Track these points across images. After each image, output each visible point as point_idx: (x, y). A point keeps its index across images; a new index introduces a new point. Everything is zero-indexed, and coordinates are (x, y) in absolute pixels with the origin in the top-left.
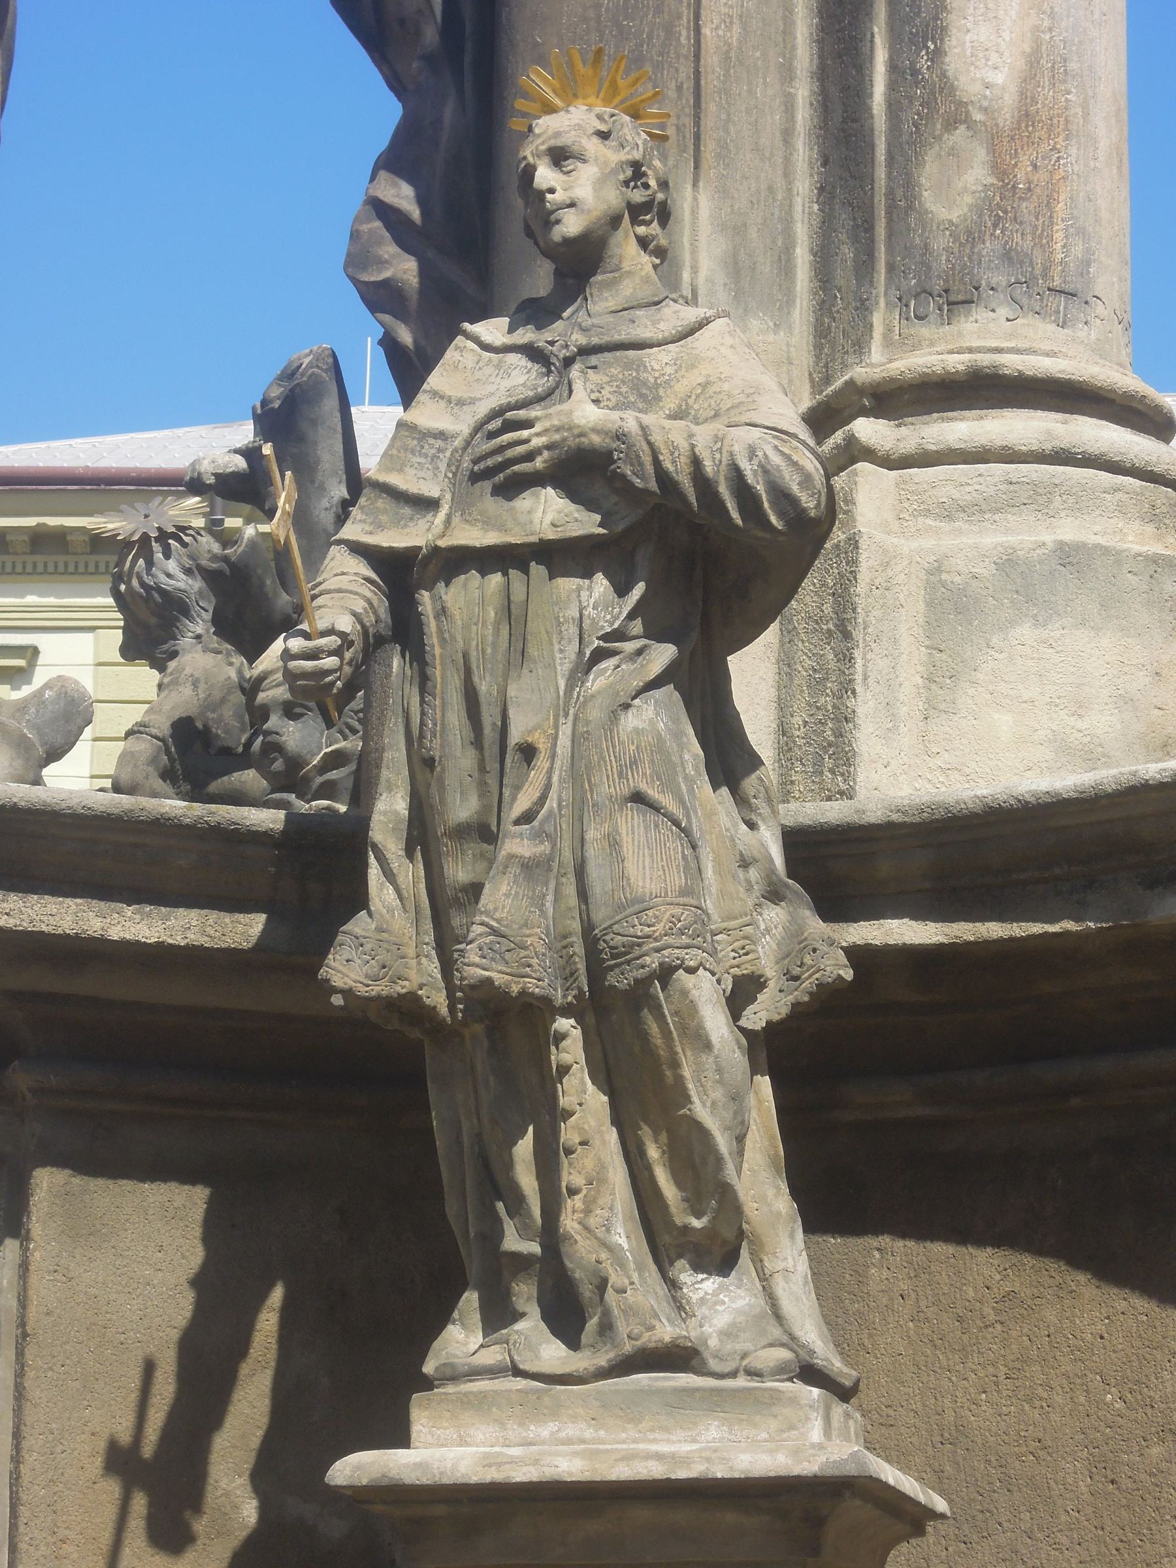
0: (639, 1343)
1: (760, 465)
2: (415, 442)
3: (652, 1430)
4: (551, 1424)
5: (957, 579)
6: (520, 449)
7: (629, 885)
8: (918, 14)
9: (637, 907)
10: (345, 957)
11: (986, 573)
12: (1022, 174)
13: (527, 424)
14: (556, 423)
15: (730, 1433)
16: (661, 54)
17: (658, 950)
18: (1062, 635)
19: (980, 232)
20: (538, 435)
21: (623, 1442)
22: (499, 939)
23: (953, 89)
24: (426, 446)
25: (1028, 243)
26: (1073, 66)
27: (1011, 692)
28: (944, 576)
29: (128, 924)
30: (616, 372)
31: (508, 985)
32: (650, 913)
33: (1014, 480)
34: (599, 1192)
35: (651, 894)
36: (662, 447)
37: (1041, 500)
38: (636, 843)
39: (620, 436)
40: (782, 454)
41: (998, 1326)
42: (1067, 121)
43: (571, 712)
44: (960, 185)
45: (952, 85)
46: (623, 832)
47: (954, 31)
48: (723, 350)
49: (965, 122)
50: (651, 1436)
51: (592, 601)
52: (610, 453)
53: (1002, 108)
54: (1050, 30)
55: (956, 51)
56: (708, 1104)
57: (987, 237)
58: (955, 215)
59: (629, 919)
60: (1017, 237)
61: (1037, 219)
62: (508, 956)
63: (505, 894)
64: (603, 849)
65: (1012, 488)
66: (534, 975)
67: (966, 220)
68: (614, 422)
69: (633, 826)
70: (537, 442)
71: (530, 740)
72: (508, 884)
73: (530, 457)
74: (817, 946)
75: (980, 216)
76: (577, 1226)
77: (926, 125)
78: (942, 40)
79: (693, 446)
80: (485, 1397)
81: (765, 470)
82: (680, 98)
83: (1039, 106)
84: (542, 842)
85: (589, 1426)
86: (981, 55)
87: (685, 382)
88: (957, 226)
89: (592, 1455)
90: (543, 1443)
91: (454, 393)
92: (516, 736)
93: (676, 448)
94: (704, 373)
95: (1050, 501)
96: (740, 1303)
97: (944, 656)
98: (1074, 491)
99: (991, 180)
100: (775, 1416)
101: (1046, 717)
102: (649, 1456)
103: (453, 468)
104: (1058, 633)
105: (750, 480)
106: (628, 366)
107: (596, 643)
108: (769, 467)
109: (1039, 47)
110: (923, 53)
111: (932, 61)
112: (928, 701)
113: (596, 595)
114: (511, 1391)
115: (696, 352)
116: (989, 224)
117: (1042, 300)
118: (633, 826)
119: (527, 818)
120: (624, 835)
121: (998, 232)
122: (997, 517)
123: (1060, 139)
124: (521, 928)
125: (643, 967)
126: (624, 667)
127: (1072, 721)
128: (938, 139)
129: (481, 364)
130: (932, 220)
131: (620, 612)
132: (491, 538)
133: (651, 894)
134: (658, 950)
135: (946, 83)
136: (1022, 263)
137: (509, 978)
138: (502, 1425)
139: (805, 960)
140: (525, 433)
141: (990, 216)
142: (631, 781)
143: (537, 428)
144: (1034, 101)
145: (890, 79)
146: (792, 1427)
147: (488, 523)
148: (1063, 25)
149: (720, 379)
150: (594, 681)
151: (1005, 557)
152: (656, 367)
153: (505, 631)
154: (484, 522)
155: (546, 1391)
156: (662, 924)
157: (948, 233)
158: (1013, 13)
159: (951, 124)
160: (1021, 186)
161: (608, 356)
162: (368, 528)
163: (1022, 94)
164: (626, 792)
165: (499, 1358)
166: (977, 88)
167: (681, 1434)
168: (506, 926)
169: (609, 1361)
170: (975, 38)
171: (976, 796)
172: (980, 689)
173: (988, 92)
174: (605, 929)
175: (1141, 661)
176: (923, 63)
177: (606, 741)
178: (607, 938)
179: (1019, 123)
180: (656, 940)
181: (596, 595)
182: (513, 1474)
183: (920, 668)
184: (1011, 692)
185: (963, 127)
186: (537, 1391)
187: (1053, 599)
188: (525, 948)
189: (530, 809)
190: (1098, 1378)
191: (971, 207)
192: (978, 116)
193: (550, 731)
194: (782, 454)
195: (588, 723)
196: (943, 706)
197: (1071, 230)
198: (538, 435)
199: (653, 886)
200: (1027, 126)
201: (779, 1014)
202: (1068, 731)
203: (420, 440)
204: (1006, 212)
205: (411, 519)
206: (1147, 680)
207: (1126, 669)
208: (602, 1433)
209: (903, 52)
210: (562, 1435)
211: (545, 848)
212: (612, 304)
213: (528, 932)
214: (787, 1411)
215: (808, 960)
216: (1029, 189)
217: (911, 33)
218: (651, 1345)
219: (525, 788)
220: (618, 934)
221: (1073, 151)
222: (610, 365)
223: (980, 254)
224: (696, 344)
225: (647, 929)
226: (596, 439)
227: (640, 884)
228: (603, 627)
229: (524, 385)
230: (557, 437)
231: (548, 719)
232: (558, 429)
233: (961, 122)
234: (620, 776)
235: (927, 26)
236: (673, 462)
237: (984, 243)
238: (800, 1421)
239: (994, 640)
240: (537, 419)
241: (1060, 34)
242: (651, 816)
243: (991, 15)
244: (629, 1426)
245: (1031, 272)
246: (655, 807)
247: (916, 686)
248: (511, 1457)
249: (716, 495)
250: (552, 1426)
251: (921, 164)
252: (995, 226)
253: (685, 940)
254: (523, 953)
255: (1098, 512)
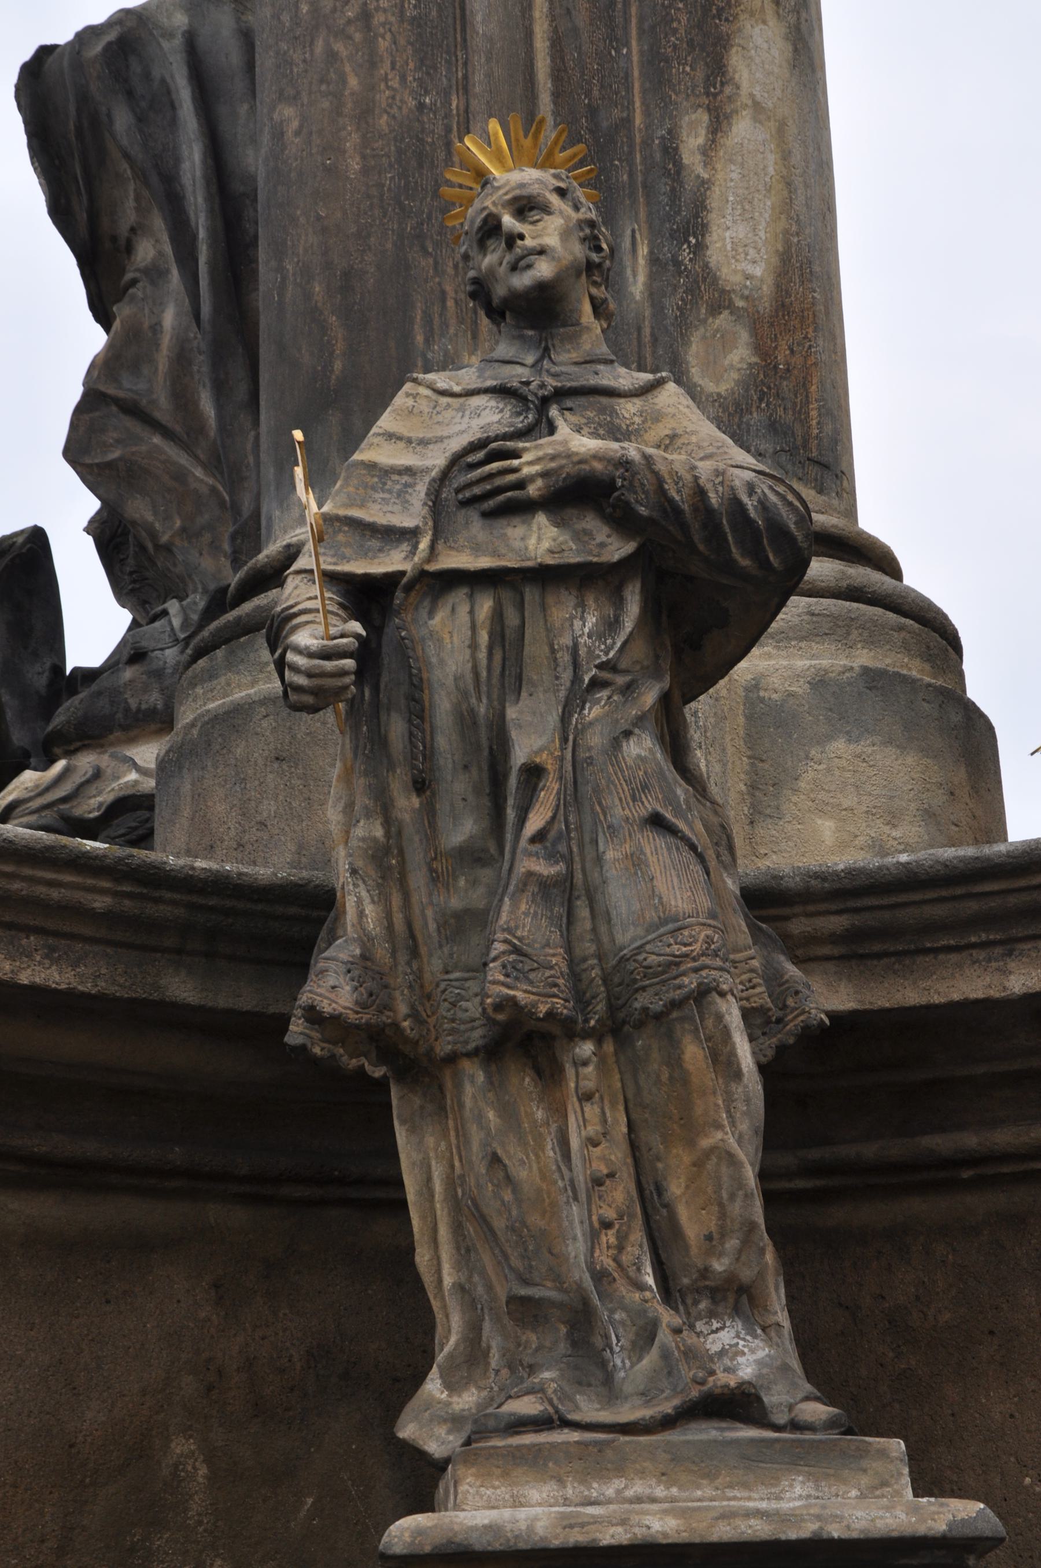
0: (705, 1388)
1: (760, 501)
2: (376, 479)
3: (731, 1486)
4: (617, 1481)
5: (774, 696)
6: (511, 478)
7: (662, 904)
8: (678, 213)
9: (671, 926)
10: (331, 983)
11: (800, 691)
12: (782, 356)
13: (516, 454)
14: (550, 451)
15: (817, 1490)
16: (440, 234)
17: (696, 970)
18: (874, 751)
19: (747, 404)
20: (530, 463)
21: (699, 1500)
22: (521, 958)
23: (715, 279)
24: (389, 483)
25: (790, 417)
26: (816, 268)
27: (831, 800)
28: (762, 694)
29: (37, 968)
30: (592, 415)
31: (534, 1005)
32: (686, 933)
33: (816, 612)
34: (629, 1227)
35: (684, 914)
36: (666, 476)
37: (840, 631)
38: (661, 863)
39: (625, 463)
40: (777, 493)
41: (897, 1406)
42: (814, 316)
43: (571, 737)
44: (727, 362)
45: (715, 275)
46: (648, 852)
47: (714, 228)
48: (681, 408)
49: (728, 307)
50: (730, 1493)
51: (586, 630)
52: (613, 481)
53: (761, 298)
54: (798, 234)
55: (717, 245)
56: (736, 1136)
57: (754, 409)
58: (723, 388)
59: (664, 938)
60: (780, 411)
61: (796, 397)
62: (532, 976)
63: (524, 913)
64: (627, 869)
65: (814, 619)
66: (561, 995)
67: (734, 393)
68: (616, 451)
69: (656, 847)
70: (526, 471)
71: (538, 760)
72: (527, 903)
73: (521, 485)
74: (800, 988)
75: (747, 390)
76: (611, 1263)
77: (691, 309)
78: (703, 236)
79: (696, 478)
80: (540, 1450)
81: (763, 505)
82: (456, 275)
83: (793, 299)
84: (557, 862)
85: (659, 1482)
86: (741, 250)
87: (653, 433)
88: (725, 398)
89: (682, 1513)
90: (609, 1502)
91: (417, 434)
92: (520, 755)
93: (680, 478)
94: (669, 426)
95: (848, 633)
96: (761, 1354)
97: (766, 766)
98: (868, 625)
99: (755, 359)
100: (865, 1471)
101: (864, 824)
102: (748, 1514)
103: (433, 497)
104: (870, 750)
105: (752, 514)
106: (602, 410)
107: (594, 671)
108: (768, 504)
109: (790, 247)
110: (685, 246)
111: (694, 253)
112: (753, 806)
113: (589, 625)
114: (568, 1443)
115: (658, 407)
116: (755, 397)
117: (803, 468)
118: (656, 847)
119: (539, 837)
120: (649, 854)
121: (763, 405)
122: (803, 644)
123: (810, 330)
124: (543, 947)
125: (680, 987)
126: (615, 698)
127: (886, 829)
128: (704, 322)
129: (438, 409)
130: (701, 393)
131: (614, 643)
132: (484, 562)
133: (684, 914)
134: (696, 970)
135: (708, 274)
136: (785, 434)
137: (536, 998)
138: (561, 1482)
139: (788, 1003)
140: (516, 462)
141: (755, 391)
142: (646, 803)
143: (527, 457)
144: (788, 294)
145: (651, 271)
146: (884, 1484)
147: (477, 549)
148: (807, 232)
149: (687, 432)
150: (590, 709)
151: (817, 678)
152: (627, 416)
153: (498, 657)
154: (472, 548)
155: (607, 1443)
156: (699, 944)
157: (717, 404)
158: (767, 215)
159: (715, 310)
160: (781, 367)
161: (582, 400)
162: (334, 560)
163: (778, 286)
164: (644, 813)
165: (542, 1408)
166: (738, 278)
167: (763, 1491)
168: (528, 945)
169: (676, 1408)
170: (734, 235)
171: (898, 862)
172: (802, 797)
173: (748, 283)
174: (638, 948)
175: (939, 780)
176: (685, 255)
177: (613, 766)
178: (640, 958)
179: (777, 311)
180: (694, 959)
181: (589, 625)
182: (598, 1535)
183: (743, 776)
184: (831, 800)
185: (726, 312)
186: (595, 1443)
187: (863, 718)
188: (551, 968)
189: (544, 828)
190: (1012, 1459)
191: (738, 383)
192: (740, 303)
193: (556, 753)
194: (777, 493)
195: (590, 749)
196: (768, 811)
197: (823, 410)
198: (530, 463)
199: (685, 906)
200: (783, 315)
201: (765, 1056)
202: (884, 837)
203: (380, 478)
204: (769, 388)
205: (380, 550)
206: (945, 797)
207: (928, 786)
208: (674, 1490)
209: (664, 246)
210: (629, 1493)
211: (560, 868)
212: (574, 356)
213: (551, 951)
214: (877, 1465)
215: (790, 1002)
216: (788, 370)
217: (672, 229)
218: (718, 1391)
219: (537, 807)
220: (653, 953)
221: (821, 342)
222: (586, 409)
223: (748, 425)
224: (656, 400)
225: (684, 949)
226: (598, 466)
227: (673, 903)
228: (599, 656)
229: (499, 422)
230: (553, 465)
231: (553, 741)
232: (553, 458)
233: (725, 308)
234: (634, 799)
235: (688, 223)
236: (679, 491)
237: (751, 414)
238: (892, 1476)
239: (813, 752)
240: (525, 449)
241: (805, 239)
242: (670, 839)
243: (748, 216)
244: (705, 1482)
245: (794, 443)
246: (672, 830)
247: (741, 793)
248: (593, 1516)
249: (718, 527)
250: (618, 1483)
251: (687, 343)
252: (761, 400)
253: (718, 963)
254: (548, 973)
255: (888, 647)
